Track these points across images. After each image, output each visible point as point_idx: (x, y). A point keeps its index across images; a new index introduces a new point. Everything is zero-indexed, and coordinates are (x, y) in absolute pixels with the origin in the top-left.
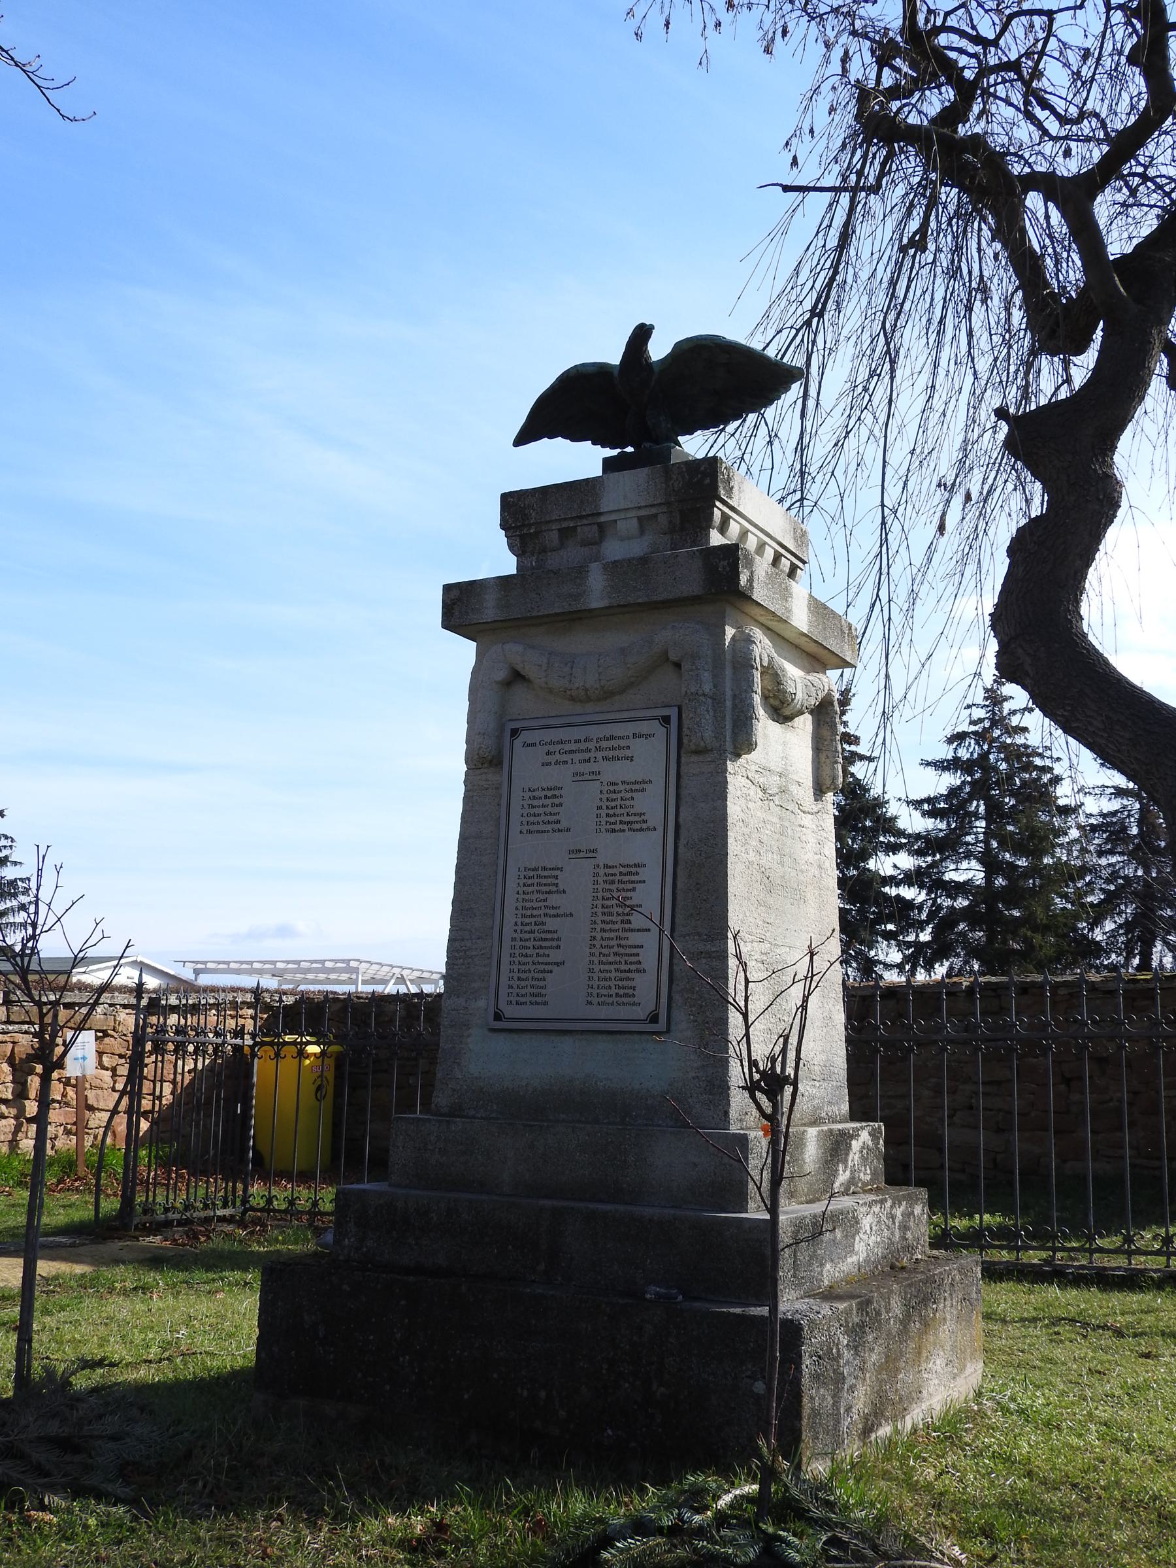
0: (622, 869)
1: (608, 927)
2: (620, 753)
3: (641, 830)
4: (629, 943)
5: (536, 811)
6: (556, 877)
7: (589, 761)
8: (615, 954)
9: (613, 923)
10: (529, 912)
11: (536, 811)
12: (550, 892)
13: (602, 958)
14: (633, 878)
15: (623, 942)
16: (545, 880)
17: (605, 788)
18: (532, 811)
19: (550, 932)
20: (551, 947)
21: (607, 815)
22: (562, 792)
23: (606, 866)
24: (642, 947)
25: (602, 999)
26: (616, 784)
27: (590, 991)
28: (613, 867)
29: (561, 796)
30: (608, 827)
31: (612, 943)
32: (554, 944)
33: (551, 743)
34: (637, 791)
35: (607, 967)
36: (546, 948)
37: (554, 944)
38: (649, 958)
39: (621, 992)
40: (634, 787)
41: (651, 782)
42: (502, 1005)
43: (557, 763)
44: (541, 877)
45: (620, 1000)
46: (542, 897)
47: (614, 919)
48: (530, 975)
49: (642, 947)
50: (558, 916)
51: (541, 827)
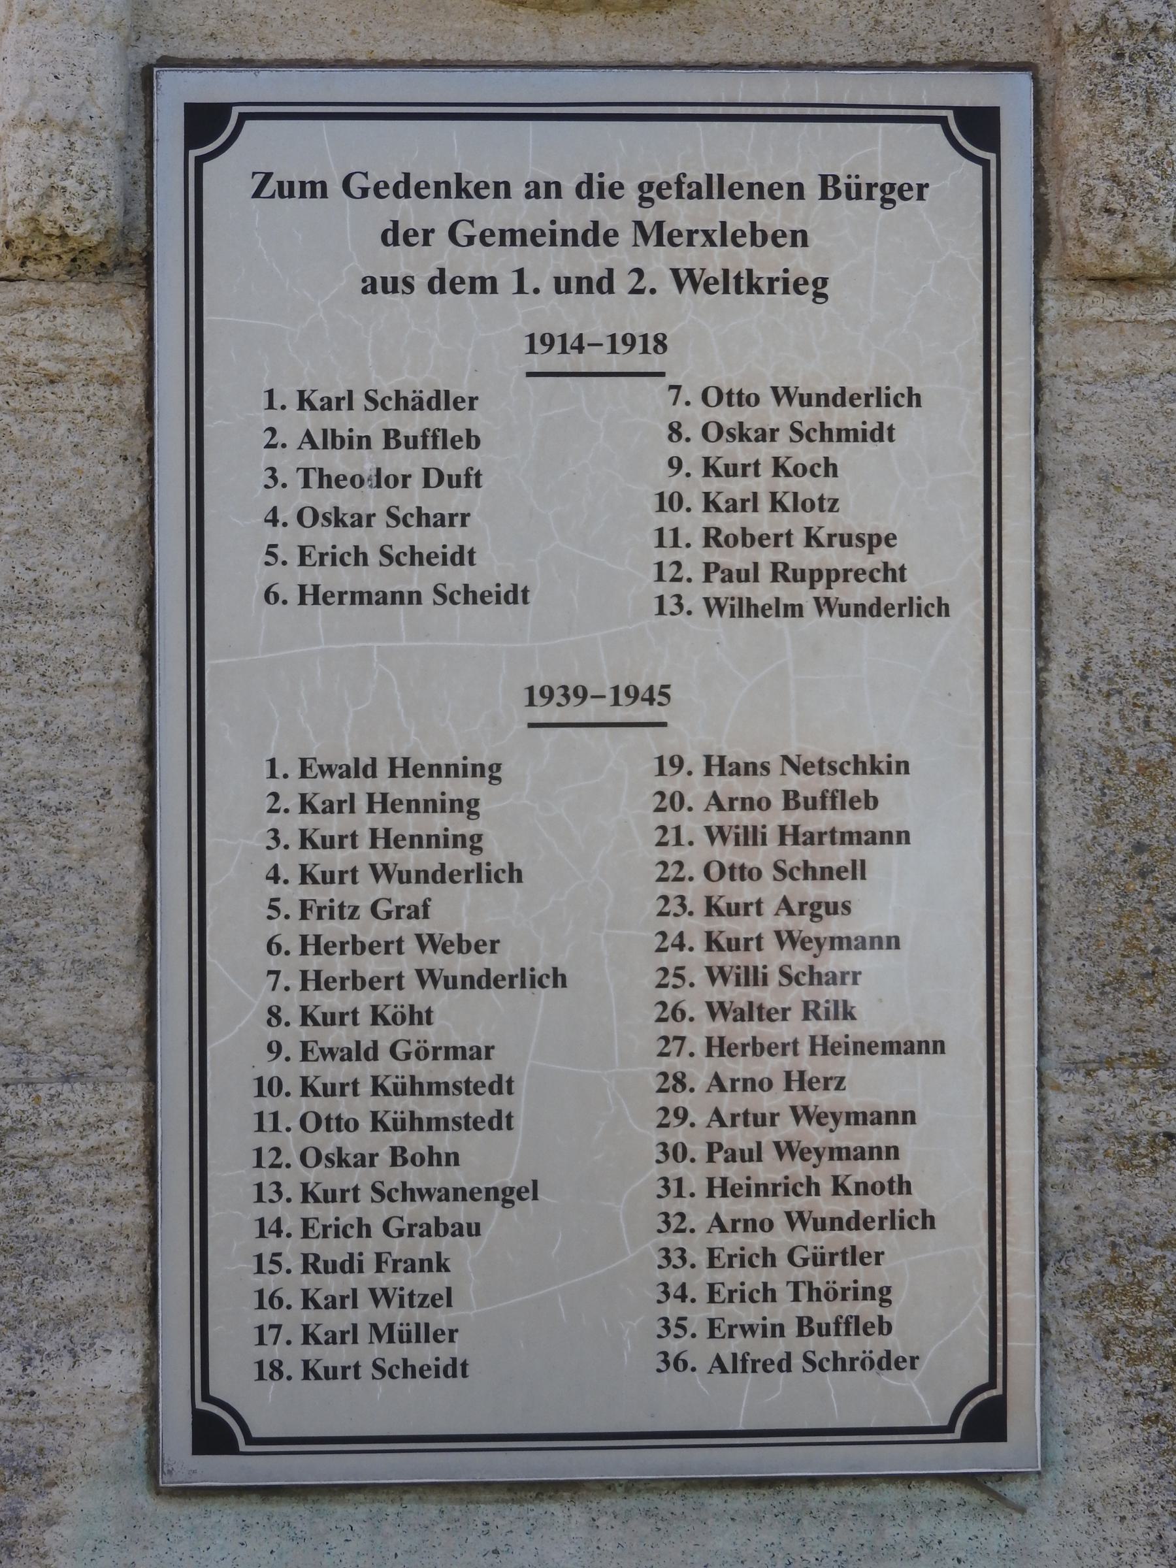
0: (794, 781)
1: (742, 1032)
2: (766, 262)
3: (877, 609)
4: (850, 1100)
5: (347, 500)
6: (471, 808)
7: (605, 284)
8: (786, 1149)
9: (765, 1014)
10: (338, 965)
11: (347, 500)
12: (442, 875)
13: (722, 1169)
14: (849, 820)
15: (819, 1100)
16: (411, 818)
17: (695, 416)
18: (326, 500)
19: (454, 1053)
20: (469, 1123)
21: (712, 537)
22: (476, 421)
23: (715, 765)
24: (909, 1117)
25: (738, 1344)
26: (744, 399)
27: (673, 1309)
28: (750, 769)
29: (472, 440)
30: (717, 589)
31: (764, 1102)
32: (483, 1106)
33: (406, 187)
34: (847, 435)
35: (748, 1207)
36: (439, 1124)
37: (483, 1106)
38: (944, 1163)
39: (825, 1312)
40: (837, 417)
41: (914, 398)
42: (232, 1381)
43: (440, 283)
44: (387, 804)
45: (822, 1347)
46: (403, 895)
47: (768, 996)
48: (369, 1248)
49: (909, 1117)
50: (489, 981)
51: (374, 578)
